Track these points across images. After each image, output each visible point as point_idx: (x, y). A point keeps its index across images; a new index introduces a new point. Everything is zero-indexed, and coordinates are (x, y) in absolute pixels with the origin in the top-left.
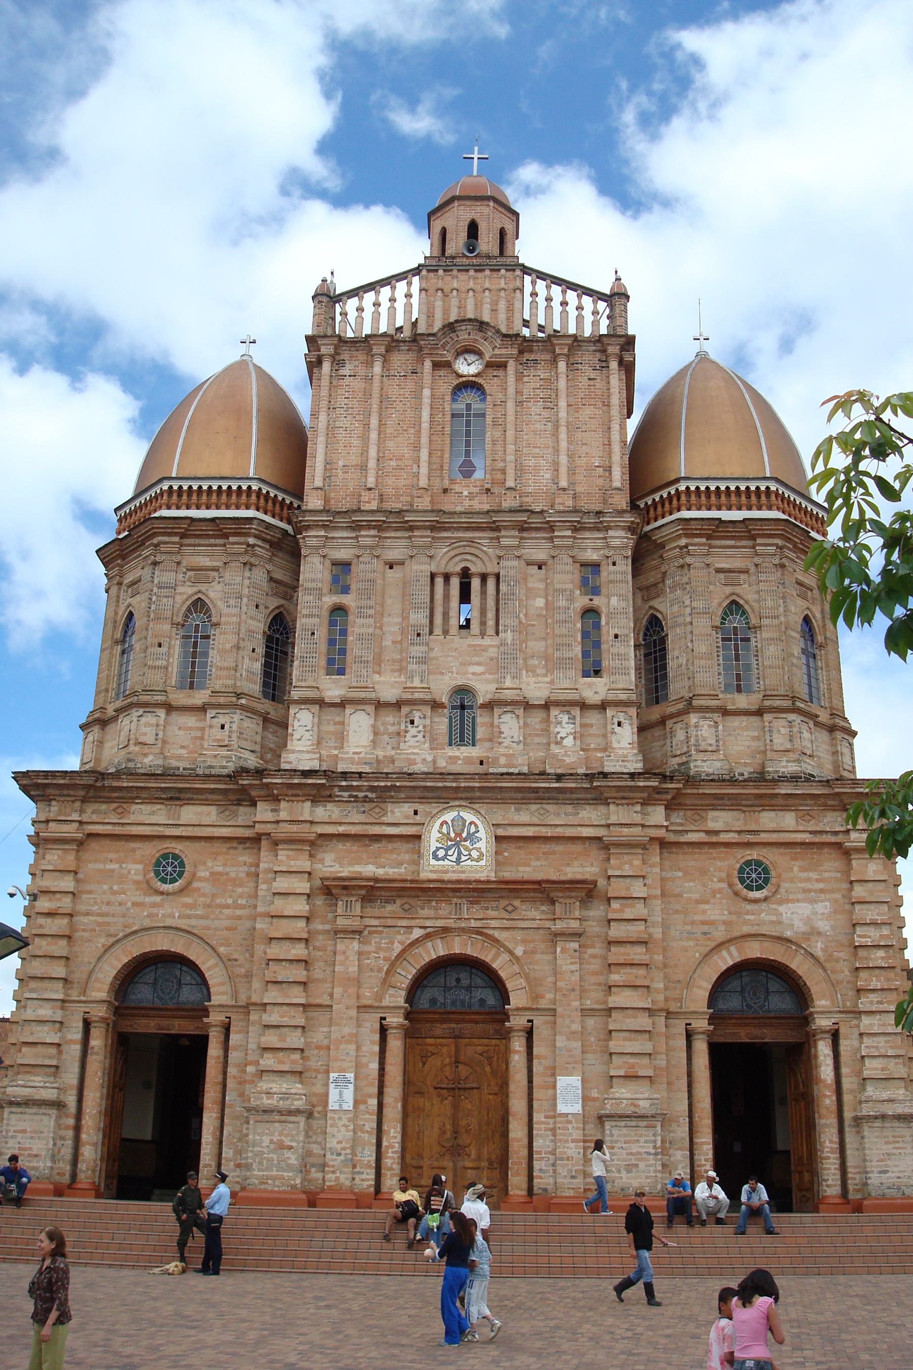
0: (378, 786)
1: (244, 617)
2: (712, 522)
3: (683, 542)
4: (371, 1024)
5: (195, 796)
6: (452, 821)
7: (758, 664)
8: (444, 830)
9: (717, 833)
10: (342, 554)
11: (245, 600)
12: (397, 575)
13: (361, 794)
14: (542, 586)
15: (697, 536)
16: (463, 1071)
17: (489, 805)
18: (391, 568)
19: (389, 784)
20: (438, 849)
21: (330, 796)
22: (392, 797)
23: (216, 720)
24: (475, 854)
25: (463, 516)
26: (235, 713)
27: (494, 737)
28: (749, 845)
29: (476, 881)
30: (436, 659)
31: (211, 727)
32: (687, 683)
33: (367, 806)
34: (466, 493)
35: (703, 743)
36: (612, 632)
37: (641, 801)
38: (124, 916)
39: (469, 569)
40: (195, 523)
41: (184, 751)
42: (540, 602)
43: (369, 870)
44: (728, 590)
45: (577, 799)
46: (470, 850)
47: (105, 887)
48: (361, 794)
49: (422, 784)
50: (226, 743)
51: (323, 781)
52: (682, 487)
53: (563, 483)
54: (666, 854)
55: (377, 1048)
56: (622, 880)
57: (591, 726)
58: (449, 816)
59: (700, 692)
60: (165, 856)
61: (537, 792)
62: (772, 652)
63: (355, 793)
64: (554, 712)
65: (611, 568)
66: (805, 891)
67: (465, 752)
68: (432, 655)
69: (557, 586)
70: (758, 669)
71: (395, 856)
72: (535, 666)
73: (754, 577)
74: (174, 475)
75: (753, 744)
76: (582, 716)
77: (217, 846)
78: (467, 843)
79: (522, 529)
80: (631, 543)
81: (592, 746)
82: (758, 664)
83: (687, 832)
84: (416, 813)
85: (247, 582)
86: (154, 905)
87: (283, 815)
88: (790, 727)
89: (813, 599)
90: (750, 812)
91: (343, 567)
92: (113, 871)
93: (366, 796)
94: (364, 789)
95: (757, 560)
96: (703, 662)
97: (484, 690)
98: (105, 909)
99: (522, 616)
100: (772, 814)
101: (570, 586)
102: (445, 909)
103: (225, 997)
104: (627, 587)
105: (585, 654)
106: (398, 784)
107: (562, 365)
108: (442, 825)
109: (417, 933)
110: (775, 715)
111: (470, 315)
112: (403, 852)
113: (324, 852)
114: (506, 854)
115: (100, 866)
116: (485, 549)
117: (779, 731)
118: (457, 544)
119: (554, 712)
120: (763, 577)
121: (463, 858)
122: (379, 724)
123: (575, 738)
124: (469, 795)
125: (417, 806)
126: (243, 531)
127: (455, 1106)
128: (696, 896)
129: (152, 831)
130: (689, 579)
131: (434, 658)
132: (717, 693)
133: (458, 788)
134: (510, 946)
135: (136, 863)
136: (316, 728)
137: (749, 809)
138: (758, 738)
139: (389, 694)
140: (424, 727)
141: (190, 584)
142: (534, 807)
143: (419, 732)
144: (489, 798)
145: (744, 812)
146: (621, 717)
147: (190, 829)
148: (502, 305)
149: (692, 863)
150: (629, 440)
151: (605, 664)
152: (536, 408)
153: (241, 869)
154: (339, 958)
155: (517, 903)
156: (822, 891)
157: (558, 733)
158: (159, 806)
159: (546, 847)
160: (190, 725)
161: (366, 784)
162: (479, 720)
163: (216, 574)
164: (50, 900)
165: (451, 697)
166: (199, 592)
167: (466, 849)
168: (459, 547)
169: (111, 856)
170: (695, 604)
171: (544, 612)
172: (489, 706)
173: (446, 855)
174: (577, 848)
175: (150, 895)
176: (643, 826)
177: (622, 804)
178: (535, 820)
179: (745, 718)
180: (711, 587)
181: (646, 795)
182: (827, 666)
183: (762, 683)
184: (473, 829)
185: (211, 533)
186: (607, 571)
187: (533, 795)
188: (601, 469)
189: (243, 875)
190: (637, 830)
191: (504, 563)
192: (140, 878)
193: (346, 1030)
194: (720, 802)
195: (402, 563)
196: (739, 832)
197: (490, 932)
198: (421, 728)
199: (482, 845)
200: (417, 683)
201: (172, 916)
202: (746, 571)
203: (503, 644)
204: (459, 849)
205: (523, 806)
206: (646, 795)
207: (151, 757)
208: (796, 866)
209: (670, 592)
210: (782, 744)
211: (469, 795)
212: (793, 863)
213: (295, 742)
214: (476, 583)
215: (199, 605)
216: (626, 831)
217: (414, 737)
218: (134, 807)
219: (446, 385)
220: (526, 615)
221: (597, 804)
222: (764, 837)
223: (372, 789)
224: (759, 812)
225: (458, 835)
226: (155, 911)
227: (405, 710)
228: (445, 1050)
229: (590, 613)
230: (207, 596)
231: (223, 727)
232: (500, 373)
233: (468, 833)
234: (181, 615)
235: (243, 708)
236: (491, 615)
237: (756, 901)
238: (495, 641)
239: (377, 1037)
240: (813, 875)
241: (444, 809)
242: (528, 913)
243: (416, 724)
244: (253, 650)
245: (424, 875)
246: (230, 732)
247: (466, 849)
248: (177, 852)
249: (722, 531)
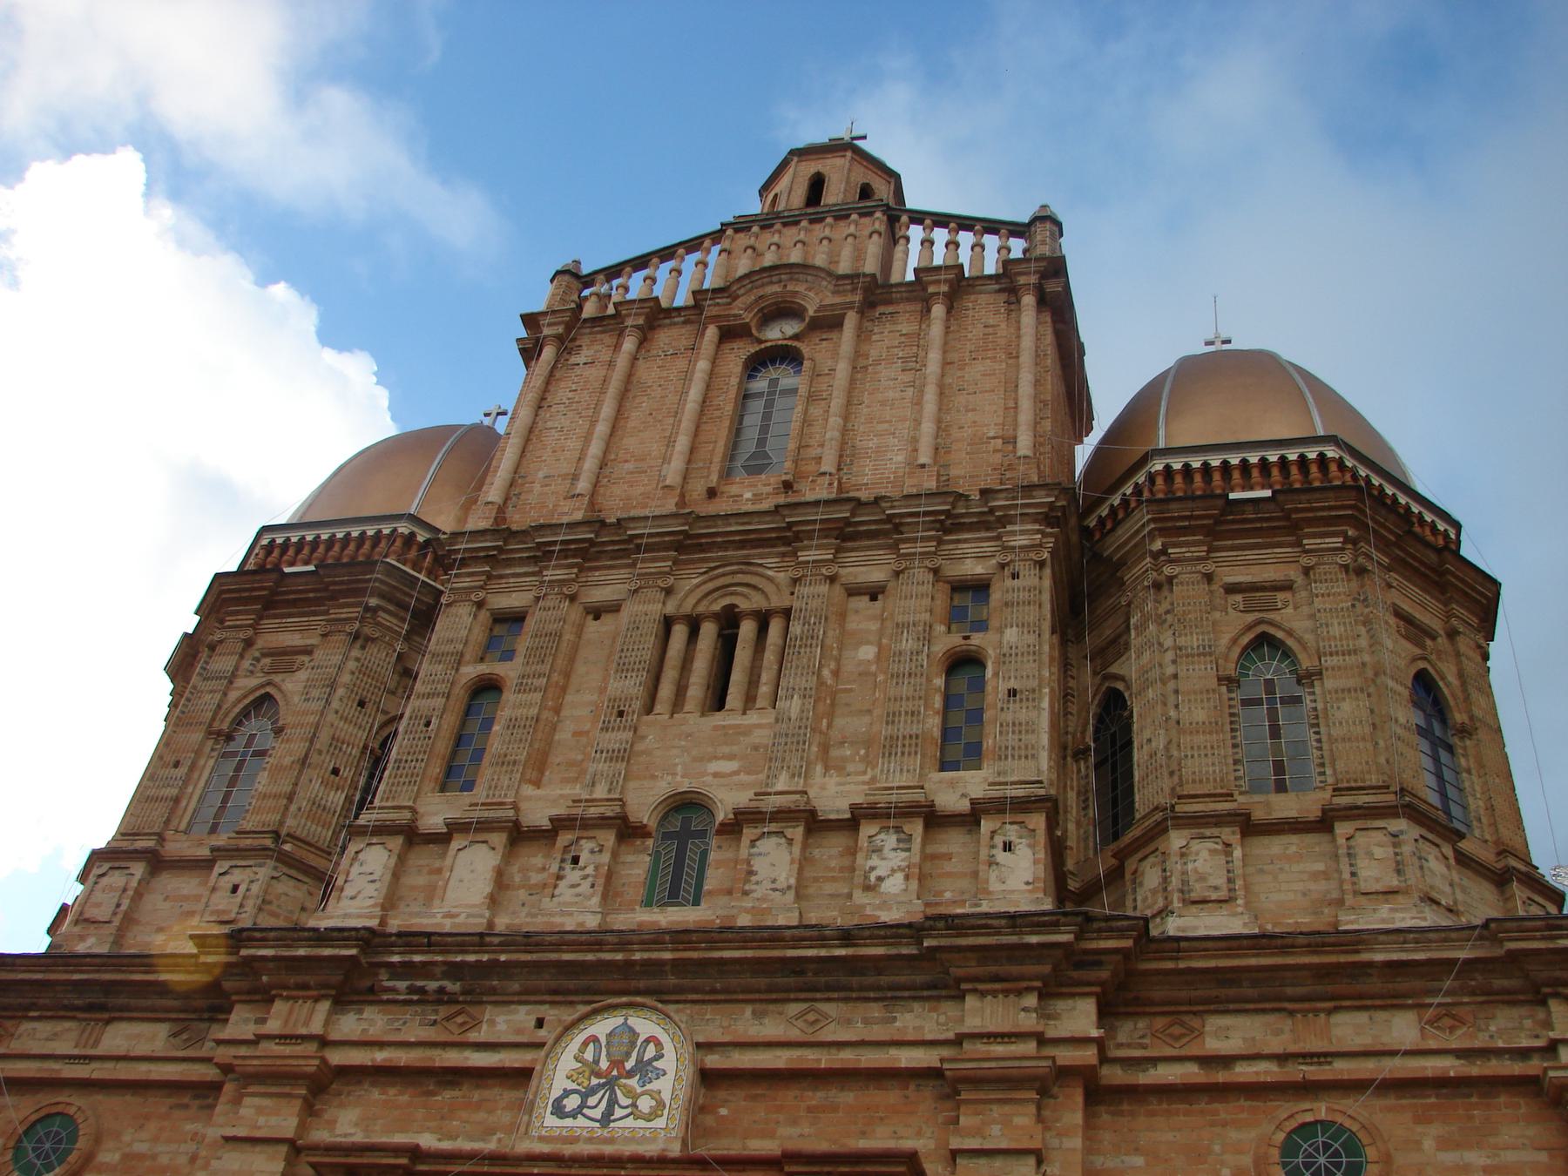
0: (463, 963)
1: (331, 717)
5: (133, 1002)
6: (610, 1035)
7: (1319, 741)
8: (589, 1055)
9: (1227, 1061)
11: (341, 692)
12: (604, 629)
13: (432, 985)
14: (874, 626)
17: (697, 1007)
18: (597, 618)
19: (485, 958)
20: (567, 1093)
21: (371, 990)
22: (493, 991)
23: (227, 878)
24: (645, 1104)
25: (732, 520)
26: (260, 866)
30: (647, 752)
31: (214, 889)
32: (1167, 783)
33: (444, 1011)
35: (1198, 886)
36: (1003, 687)
37: (1038, 984)
39: (737, 606)
42: (867, 652)
45: (890, 988)
46: (635, 1097)
48: (432, 985)
49: (553, 956)
50: (233, 916)
51: (353, 952)
52: (1158, 465)
53: (924, 458)
54: (1106, 1117)
56: (983, 1161)
57: (949, 857)
58: (602, 1027)
61: (802, 973)
62: (1348, 713)
63: (419, 983)
64: (867, 829)
65: (1009, 583)
69: (900, 619)
70: (1320, 749)
71: (481, 1116)
72: (844, 759)
73: (1304, 594)
74: (1162, 445)
75: (1313, 886)
76: (925, 841)
77: (158, 1103)
78: (633, 1082)
80: (1050, 543)
81: (948, 895)
82: (1319, 741)
83: (1154, 1061)
84: (540, 1023)
85: (352, 665)
88: (1395, 845)
89: (1439, 653)
90: (1305, 1012)
93: (441, 990)
94: (438, 970)
95: (1305, 561)
96: (1200, 739)
97: (727, 800)
99: (826, 672)
100: (1362, 1017)
101: (926, 616)
106: (503, 958)
107: (938, 310)
108: (585, 1044)
110: (1359, 824)
113: (342, 1106)
114: (723, 1111)
116: (770, 573)
117: (1370, 855)
118: (720, 570)
120: (1320, 588)
121: (619, 1113)
122: (514, 869)
123: (907, 878)
124: (653, 983)
129: (39, 1070)
130: (1172, 604)
131: (643, 752)
133: (629, 964)
136: (388, 877)
137: (1306, 1005)
138: (1326, 875)
140: (596, 868)
141: (262, 675)
142: (794, 1009)
143: (585, 877)
144: (695, 990)
145: (1292, 1013)
146: (1012, 833)
147: (109, 1065)
149: (1170, 1136)
150: (1077, 475)
151: (988, 743)
153: (183, 1147)
157: (873, 869)
158: (67, 1024)
159: (817, 1097)
160: (185, 892)
161: (439, 958)
162: (713, 856)
163: (306, 658)
165: (665, 817)
166: (269, 683)
167: (630, 1093)
168: (724, 575)
170: (1182, 641)
171: (873, 668)
173: (583, 1105)
174: (891, 1096)
176: (1041, 1039)
177: (994, 993)
178: (794, 1034)
179: (1294, 839)
180: (1217, 615)
181: (1046, 969)
182: (1481, 766)
183: (1329, 771)
184: (651, 1051)
187: (791, 980)
188: (1000, 441)
190: (1030, 1047)
191: (804, 590)
194: (1232, 992)
196: (1282, 1058)
198: (590, 870)
199: (664, 1086)
202: (1287, 586)
204: (613, 1092)
205: (771, 1007)
206: (1046, 969)
207: (91, 941)
208: (1429, 1137)
209: (1137, 635)
210: (1378, 880)
211: (653, 983)
212: (1419, 1129)
213: (345, 903)
216: (999, 1049)
217: (573, 886)
218: (26, 1026)
220: (836, 674)
221: (938, 998)
222: (1343, 1069)
223: (454, 971)
224: (1330, 1012)
225: (617, 1063)
227: (564, 838)
230: (280, 690)
231: (235, 889)
233: (639, 1061)
234: (229, 719)
235: (284, 859)
238: (769, 717)
241: (596, 1012)
243: (581, 863)
244: (335, 772)
246: (244, 897)
247: (630, 1093)
249: (1233, 522)
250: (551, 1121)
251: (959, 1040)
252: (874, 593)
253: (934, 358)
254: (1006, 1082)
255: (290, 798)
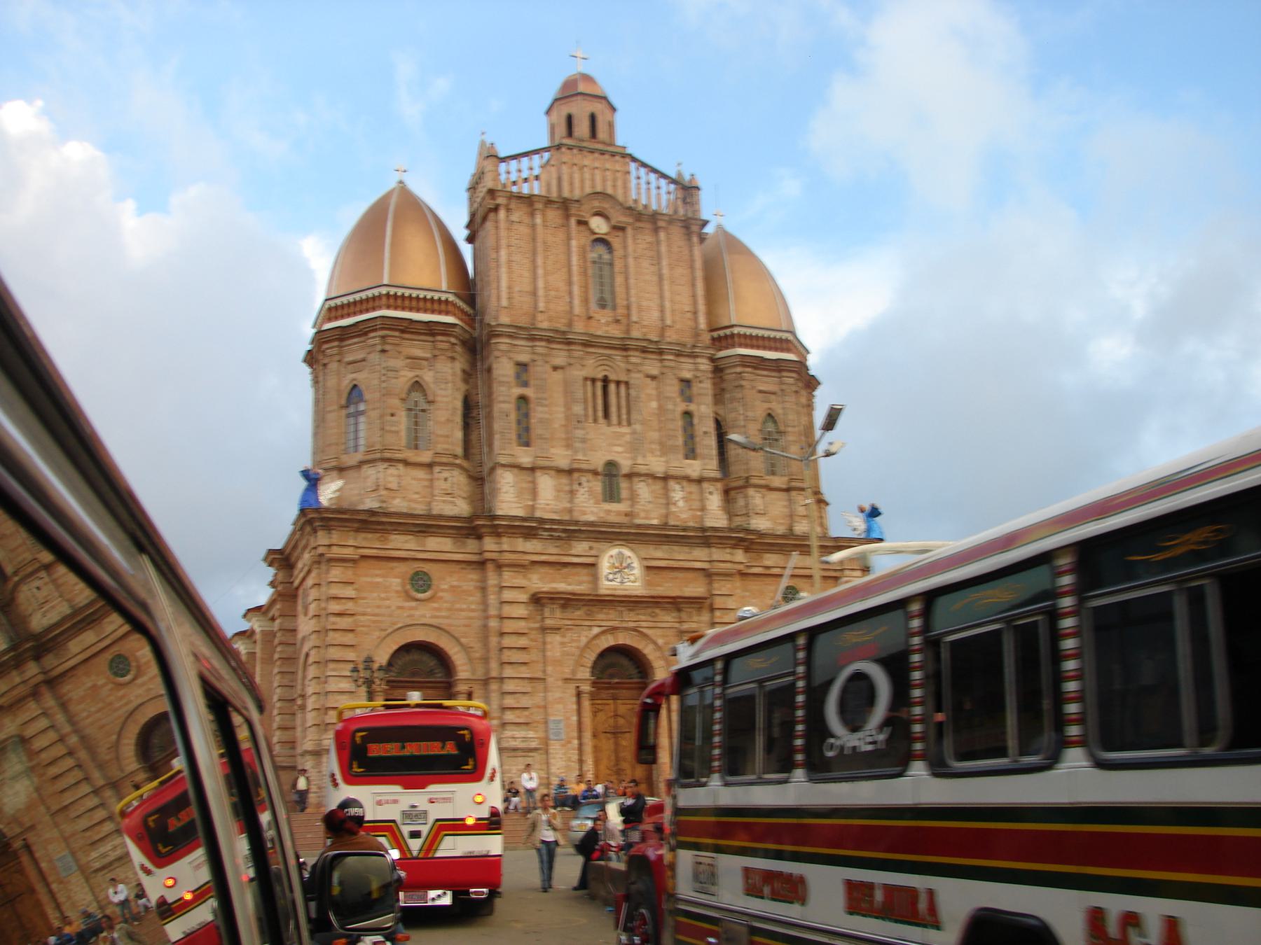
2: (757, 358)
3: (739, 369)
4: (571, 690)
10: (524, 358)
15: (749, 366)
16: (621, 721)
27: (633, 498)
29: (634, 596)
34: (603, 321)
38: (390, 616)
40: (413, 323)
41: (417, 496)
42: (654, 404)
43: (562, 586)
44: (766, 405)
47: (375, 595)
55: (575, 707)
58: (614, 551)
59: (753, 474)
60: (417, 573)
67: (614, 507)
68: (589, 437)
71: (577, 578)
79: (644, 352)
86: (412, 608)
87: (505, 547)
91: (522, 366)
92: (378, 583)
97: (625, 464)
98: (377, 611)
102: (613, 614)
103: (467, 673)
104: (709, 399)
105: (686, 443)
109: (596, 630)
111: (599, 189)
112: (583, 575)
115: (369, 579)
119: (672, 484)
120: (787, 398)
125: (591, 544)
126: (449, 333)
127: (617, 744)
132: (761, 475)
134: (654, 638)
135: (396, 577)
139: (564, 463)
142: (664, 547)
148: (620, 183)
152: (645, 264)
154: (549, 646)
155: (657, 611)
159: (676, 574)
160: (419, 477)
164: (338, 604)
169: (378, 572)
172: (630, 476)
174: (690, 575)
175: (408, 601)
178: (666, 557)
185: (422, 331)
186: (696, 388)
189: (472, 588)
190: (729, 565)
192: (399, 588)
193: (558, 695)
195: (562, 368)
197: (641, 630)
200: (580, 457)
201: (424, 616)
202: (774, 393)
203: (634, 433)
214: (612, 387)
215: (417, 385)
219: (586, 239)
223: (565, 531)
226: (412, 612)
228: (607, 707)
229: (688, 414)
232: (620, 234)
236: (624, 411)
239: (574, 699)
242: (664, 618)
248: (425, 570)
251: (330, 546)
252: (653, 378)
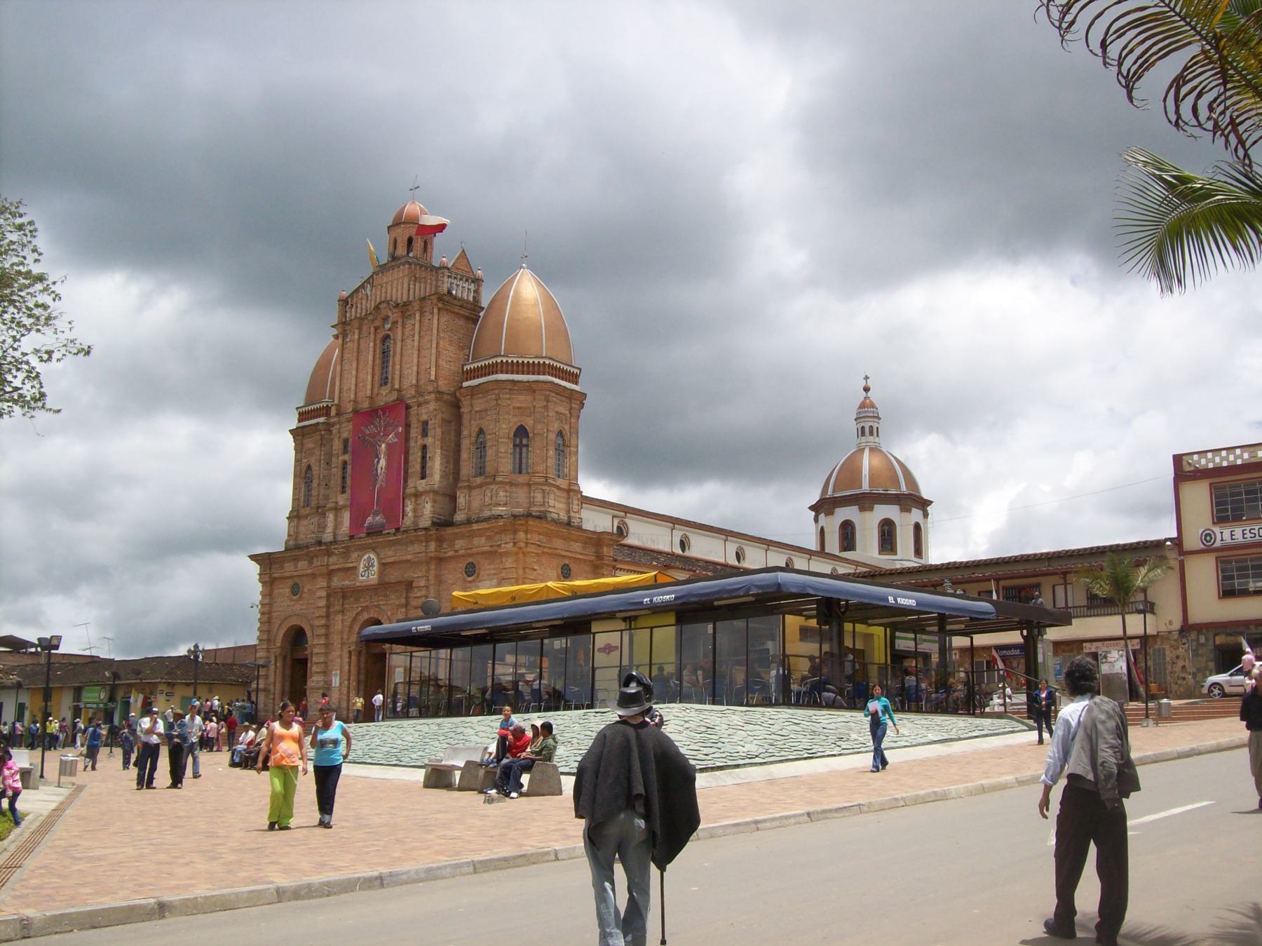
28: (471, 555)
58: (366, 557)
66: (489, 575)
76: (415, 502)
86: (293, 606)
128: (451, 582)
156: (495, 574)
169: (281, 586)
199: (375, 568)
237: (470, 582)
239: (347, 655)
240: (492, 567)
245: (358, 584)
250: (361, 578)
253: (416, 338)
254: (420, 563)
255: (319, 495)
